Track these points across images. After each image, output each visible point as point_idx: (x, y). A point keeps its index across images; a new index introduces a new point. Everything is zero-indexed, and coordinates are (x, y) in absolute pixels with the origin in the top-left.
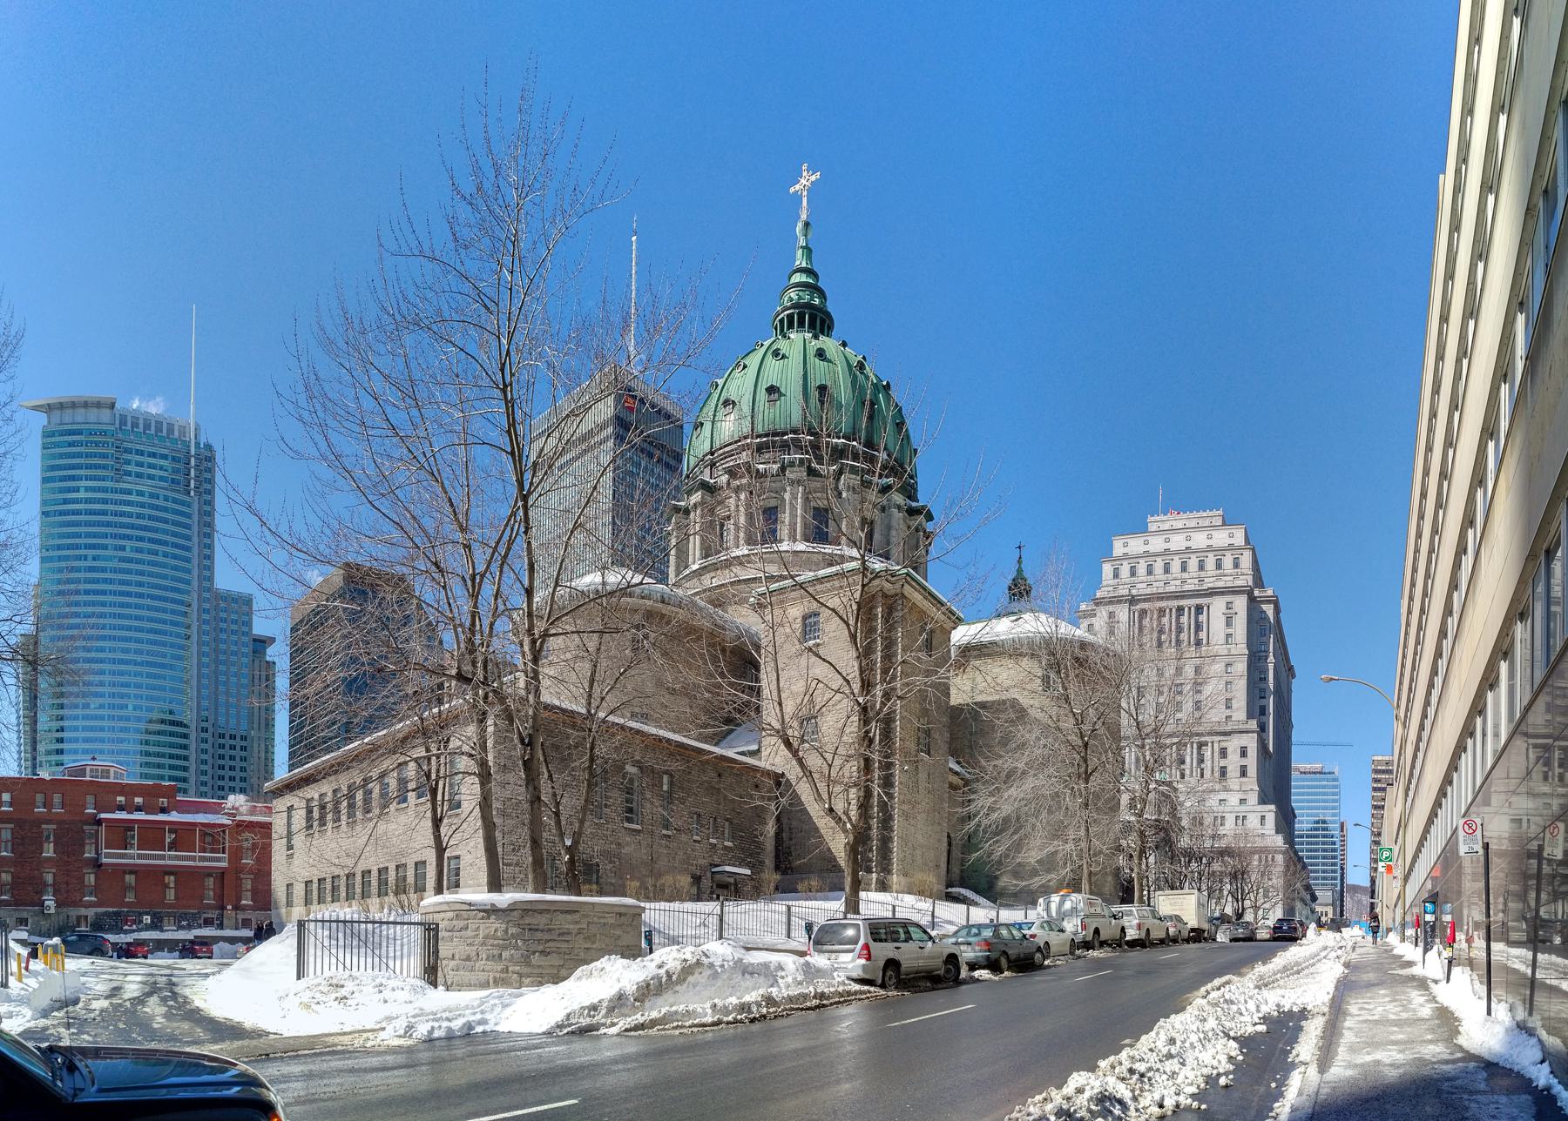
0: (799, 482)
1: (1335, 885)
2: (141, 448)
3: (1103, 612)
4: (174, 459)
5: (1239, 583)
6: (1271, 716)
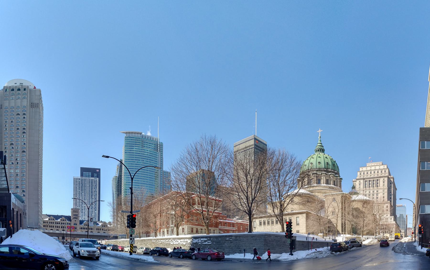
0: (324, 176)
1: (405, 229)
2: (147, 142)
3: (358, 181)
4: (154, 145)
5: (385, 175)
6: (392, 199)
